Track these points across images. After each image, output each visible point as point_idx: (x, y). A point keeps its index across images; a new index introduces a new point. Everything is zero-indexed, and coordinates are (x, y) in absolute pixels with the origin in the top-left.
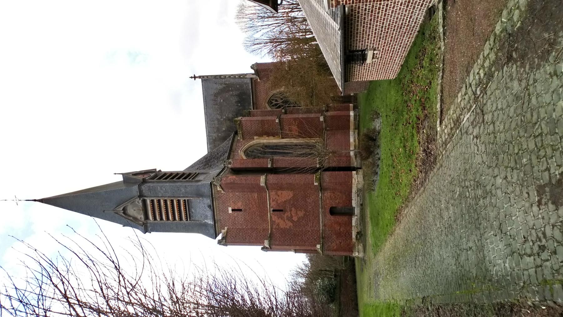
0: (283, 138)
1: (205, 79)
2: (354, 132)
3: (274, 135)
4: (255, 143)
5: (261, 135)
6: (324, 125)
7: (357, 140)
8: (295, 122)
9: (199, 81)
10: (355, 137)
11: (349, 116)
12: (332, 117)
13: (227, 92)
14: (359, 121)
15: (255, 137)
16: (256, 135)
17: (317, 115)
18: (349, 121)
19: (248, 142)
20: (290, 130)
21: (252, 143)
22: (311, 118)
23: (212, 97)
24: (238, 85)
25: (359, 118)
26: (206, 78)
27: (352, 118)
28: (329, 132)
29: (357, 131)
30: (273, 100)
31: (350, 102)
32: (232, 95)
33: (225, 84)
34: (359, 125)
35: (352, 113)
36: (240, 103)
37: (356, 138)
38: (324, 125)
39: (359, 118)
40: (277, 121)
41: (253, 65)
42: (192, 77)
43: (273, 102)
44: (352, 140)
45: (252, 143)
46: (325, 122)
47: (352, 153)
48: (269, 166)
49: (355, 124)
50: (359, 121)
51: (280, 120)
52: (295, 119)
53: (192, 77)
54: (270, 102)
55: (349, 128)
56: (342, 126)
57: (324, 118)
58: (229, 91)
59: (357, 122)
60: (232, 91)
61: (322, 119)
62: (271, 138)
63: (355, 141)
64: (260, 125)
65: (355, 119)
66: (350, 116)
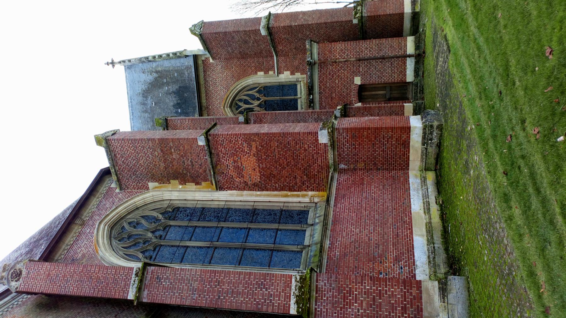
0: (220, 188)
1: (130, 65)
2: (424, 180)
3: (196, 179)
4: (149, 200)
5: (164, 178)
6: (330, 156)
7: (435, 208)
8: (250, 146)
9: (120, 68)
10: (426, 196)
11: (407, 129)
12: (356, 133)
13: (160, 88)
14: (439, 145)
15: (151, 185)
16: (154, 178)
17: (311, 127)
18: (406, 144)
19: (132, 195)
20: (239, 170)
21: (139, 199)
22: (292, 134)
23: (140, 98)
24: (177, 71)
25: (441, 137)
26: (127, 63)
27: (416, 138)
28: (344, 177)
29: (431, 176)
30: (240, 100)
31: (405, 99)
32: (168, 93)
33: (157, 72)
34: (438, 157)
35: (416, 123)
36: (180, 108)
37: (432, 199)
38: (330, 156)
39: (441, 137)
40: (202, 142)
41: (195, 26)
42: (108, 64)
43: (241, 104)
44: (417, 205)
45: (139, 199)
46: (333, 146)
47: (422, 272)
48: (131, 296)
49: (425, 154)
50: (439, 145)
51: (208, 140)
52: (248, 138)
53: (108, 64)
54: (234, 105)
55: (405, 166)
56: (385, 158)
57: (331, 135)
58: (163, 84)
59: (432, 150)
60: (168, 84)
61: (323, 138)
62: (191, 186)
63: (427, 210)
64: (158, 152)
65: (426, 140)
66: (409, 128)
